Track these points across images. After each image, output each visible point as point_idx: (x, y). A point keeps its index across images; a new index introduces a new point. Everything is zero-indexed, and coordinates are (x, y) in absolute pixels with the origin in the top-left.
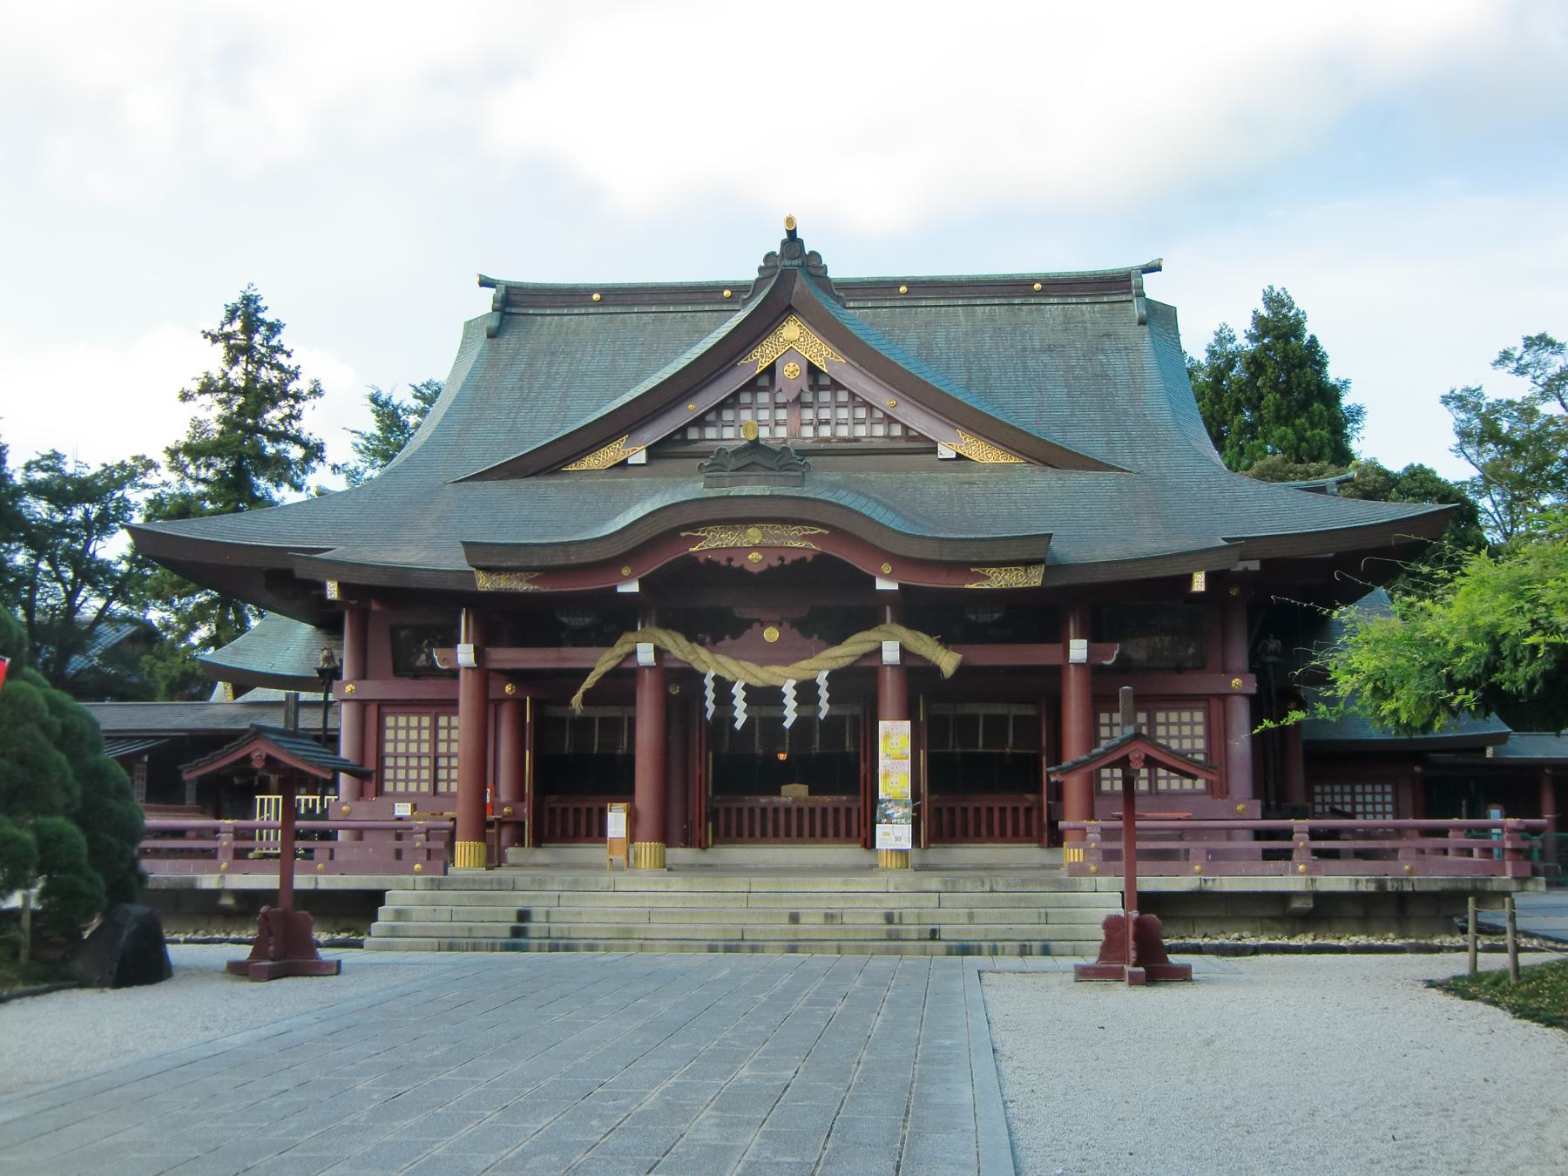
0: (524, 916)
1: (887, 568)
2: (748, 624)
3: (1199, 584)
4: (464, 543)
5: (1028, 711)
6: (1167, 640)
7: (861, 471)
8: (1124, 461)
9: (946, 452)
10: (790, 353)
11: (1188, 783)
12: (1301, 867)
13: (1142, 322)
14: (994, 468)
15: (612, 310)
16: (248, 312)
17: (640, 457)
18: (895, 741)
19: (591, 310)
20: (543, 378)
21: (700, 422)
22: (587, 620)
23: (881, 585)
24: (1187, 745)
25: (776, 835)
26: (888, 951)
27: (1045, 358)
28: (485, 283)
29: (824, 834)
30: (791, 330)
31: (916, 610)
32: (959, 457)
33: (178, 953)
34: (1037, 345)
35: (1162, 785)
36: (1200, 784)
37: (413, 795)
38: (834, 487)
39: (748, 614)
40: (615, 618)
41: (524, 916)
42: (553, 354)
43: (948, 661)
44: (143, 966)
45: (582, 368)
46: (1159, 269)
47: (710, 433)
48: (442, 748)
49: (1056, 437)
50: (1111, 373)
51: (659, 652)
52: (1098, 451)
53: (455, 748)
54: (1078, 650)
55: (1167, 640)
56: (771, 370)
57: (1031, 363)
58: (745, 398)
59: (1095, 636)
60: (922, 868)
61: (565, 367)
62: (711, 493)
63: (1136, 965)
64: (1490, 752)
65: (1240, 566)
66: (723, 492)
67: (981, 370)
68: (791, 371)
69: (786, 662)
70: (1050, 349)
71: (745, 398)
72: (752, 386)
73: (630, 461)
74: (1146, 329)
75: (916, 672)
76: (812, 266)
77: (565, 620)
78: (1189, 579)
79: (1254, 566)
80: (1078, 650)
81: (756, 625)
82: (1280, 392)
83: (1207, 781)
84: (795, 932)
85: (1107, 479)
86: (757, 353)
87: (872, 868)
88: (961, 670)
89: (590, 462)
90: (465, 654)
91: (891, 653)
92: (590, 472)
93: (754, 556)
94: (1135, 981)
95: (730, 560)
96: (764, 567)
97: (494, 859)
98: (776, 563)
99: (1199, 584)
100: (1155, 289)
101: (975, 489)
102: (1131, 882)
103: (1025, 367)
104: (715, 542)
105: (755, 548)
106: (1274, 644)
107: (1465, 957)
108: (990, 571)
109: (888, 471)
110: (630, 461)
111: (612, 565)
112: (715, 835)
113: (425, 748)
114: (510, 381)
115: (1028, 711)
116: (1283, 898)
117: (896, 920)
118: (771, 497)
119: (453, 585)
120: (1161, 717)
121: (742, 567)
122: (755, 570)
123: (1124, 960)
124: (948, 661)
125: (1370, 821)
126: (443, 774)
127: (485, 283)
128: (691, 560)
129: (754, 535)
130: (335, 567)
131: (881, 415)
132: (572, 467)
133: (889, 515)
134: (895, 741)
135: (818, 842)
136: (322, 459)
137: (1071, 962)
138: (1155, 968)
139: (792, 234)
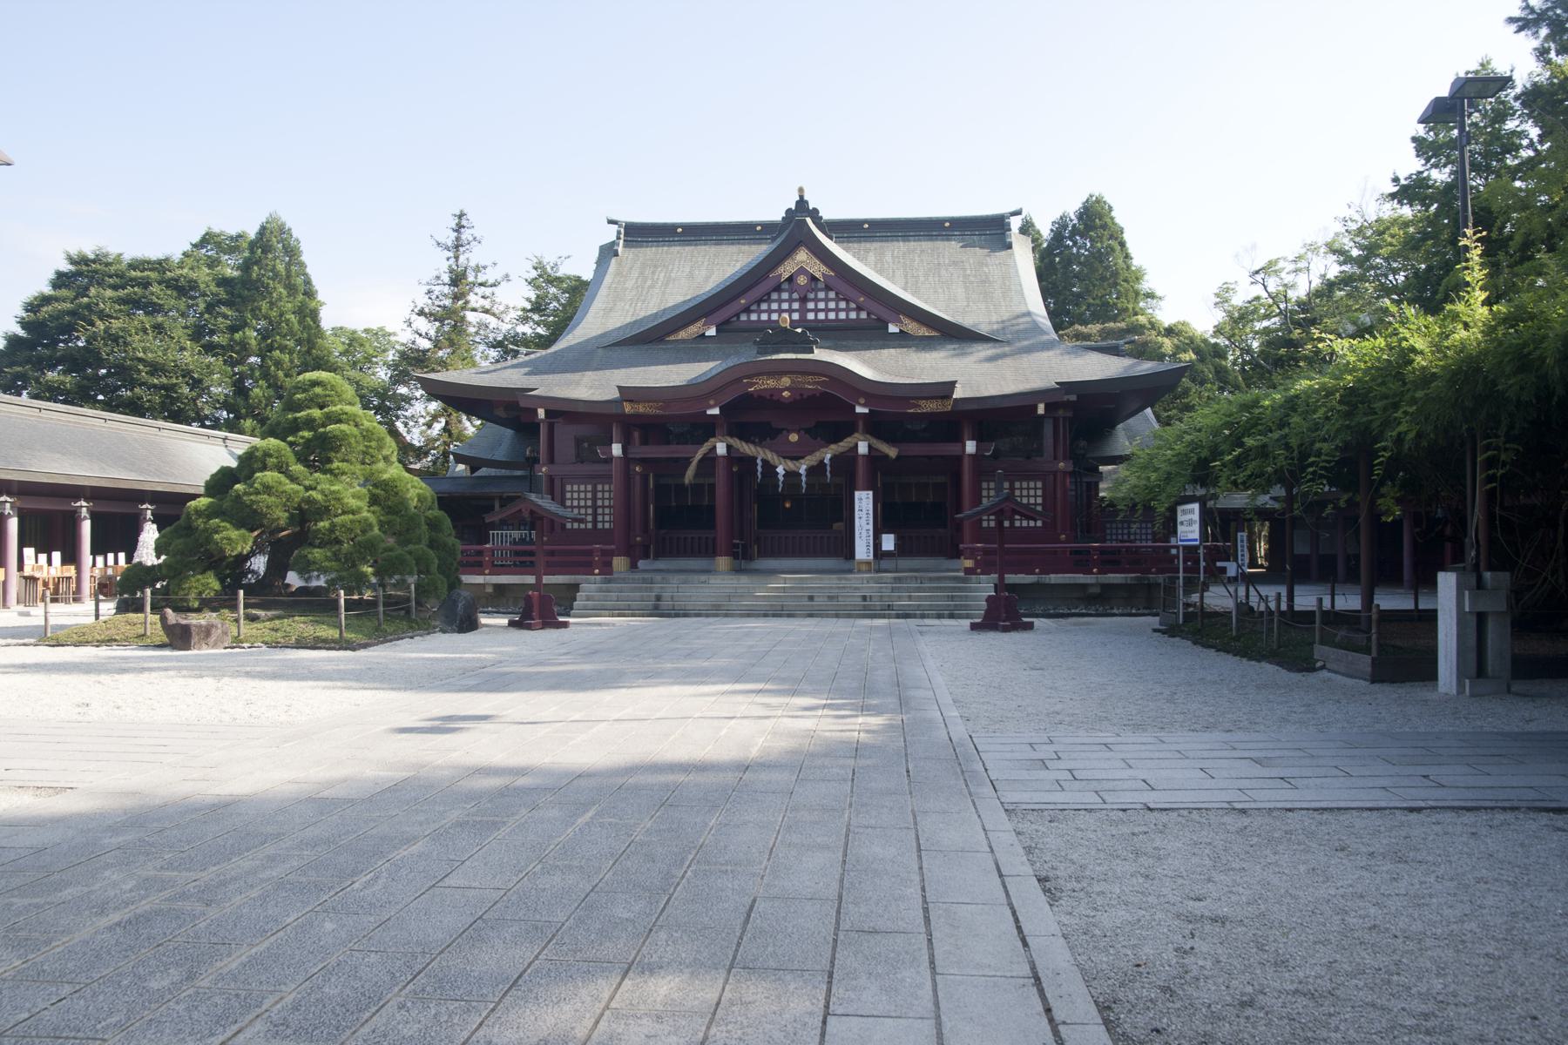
0: (658, 598)
1: (862, 401)
2: (779, 431)
3: (1041, 409)
5: (940, 479)
10: (802, 271)
11: (1032, 524)
17: (712, 332)
18: (864, 502)
21: (747, 310)
23: (859, 410)
24: (1032, 501)
28: (611, 222)
30: (802, 256)
31: (876, 426)
33: (484, 620)
35: (1017, 524)
36: (1039, 523)
40: (707, 429)
41: (658, 598)
43: (892, 452)
44: (467, 624)
47: (754, 317)
48: (599, 503)
51: (729, 447)
54: (971, 447)
56: (790, 279)
58: (775, 296)
59: (979, 439)
60: (878, 571)
65: (1066, 398)
71: (775, 296)
75: (874, 457)
78: (1035, 408)
79: (1073, 398)
80: (971, 447)
82: (1084, 267)
86: (781, 270)
87: (850, 571)
88: (898, 457)
89: (682, 335)
90: (617, 449)
92: (683, 341)
97: (633, 566)
99: (1041, 409)
102: (1001, 578)
105: (786, 389)
106: (1083, 443)
107: (815, 721)
108: (923, 403)
113: (589, 503)
114: (629, 284)
115: (940, 479)
116: (1084, 586)
124: (892, 452)
125: (1026, 343)
126: (600, 518)
127: (611, 222)
128: (750, 395)
129: (786, 381)
132: (672, 338)
134: (864, 502)
137: (966, 623)
139: (801, 197)
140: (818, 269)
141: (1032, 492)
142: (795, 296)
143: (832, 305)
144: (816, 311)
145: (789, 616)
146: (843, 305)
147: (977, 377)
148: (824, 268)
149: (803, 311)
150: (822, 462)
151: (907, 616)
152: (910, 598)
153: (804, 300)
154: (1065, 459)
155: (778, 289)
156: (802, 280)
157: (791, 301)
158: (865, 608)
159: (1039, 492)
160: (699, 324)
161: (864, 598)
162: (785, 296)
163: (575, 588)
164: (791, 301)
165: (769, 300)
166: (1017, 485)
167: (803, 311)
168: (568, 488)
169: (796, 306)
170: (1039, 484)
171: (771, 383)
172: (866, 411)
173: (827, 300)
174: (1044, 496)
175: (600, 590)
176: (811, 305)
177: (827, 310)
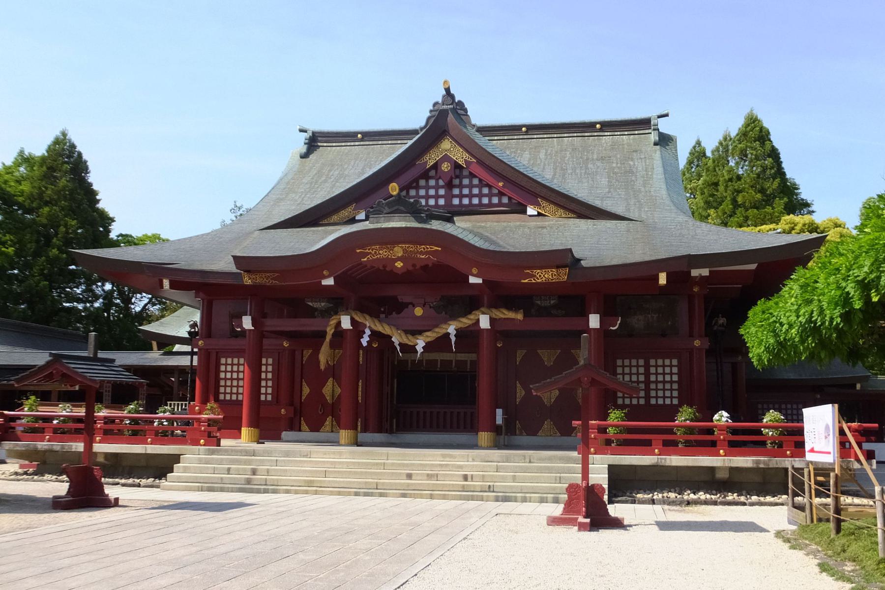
1: (475, 271)
2: (406, 305)
3: (663, 279)
4: (235, 257)
6: (655, 316)
7: (482, 222)
10: (446, 158)
12: (721, 451)
13: (656, 144)
15: (367, 143)
19: (357, 143)
20: (323, 178)
22: (323, 304)
23: (473, 280)
25: (458, 427)
26: (461, 498)
27: (599, 164)
29: (458, 427)
30: (446, 145)
34: (595, 156)
37: (627, 406)
39: (406, 299)
42: (333, 166)
45: (346, 172)
46: (667, 115)
49: (597, 203)
50: (634, 170)
52: (620, 210)
53: (241, 375)
55: (655, 316)
56: (436, 166)
57: (590, 166)
58: (422, 182)
61: (337, 172)
63: (585, 517)
64: (858, 386)
67: (562, 169)
70: (602, 159)
71: (422, 182)
73: (357, 218)
74: (658, 147)
76: (459, 110)
77: (310, 304)
81: (410, 306)
84: (408, 485)
91: (484, 322)
94: (582, 527)
95: (384, 266)
96: (405, 270)
98: (411, 268)
99: (663, 279)
100: (664, 126)
101: (545, 230)
103: (587, 168)
104: (377, 254)
105: (399, 259)
110: (357, 218)
112: (397, 426)
116: (712, 470)
117: (469, 479)
119: (230, 281)
120: (652, 362)
121: (392, 271)
123: (579, 513)
127: (301, 131)
129: (398, 251)
131: (497, 191)
133: (476, 239)
135: (447, 431)
138: (601, 521)
139: (448, 90)
140: (460, 156)
141: (667, 370)
142: (441, 183)
143: (476, 191)
144: (461, 196)
145: (381, 495)
146: (486, 191)
147: (598, 245)
148: (466, 156)
149: (449, 197)
150: (448, 335)
151: (506, 499)
152: (514, 479)
153: (449, 186)
154: (700, 337)
155: (425, 175)
156: (445, 167)
157: (437, 187)
158: (464, 489)
159: (675, 370)
160: (349, 209)
161: (465, 478)
162: (432, 182)
163: (176, 458)
164: (437, 187)
165: (417, 188)
166: (652, 362)
167: (449, 197)
168: (223, 361)
169: (442, 192)
170: (675, 362)
171: (383, 253)
172: (480, 281)
173: (471, 186)
174: (679, 374)
175: (200, 461)
176: (456, 191)
177: (471, 196)
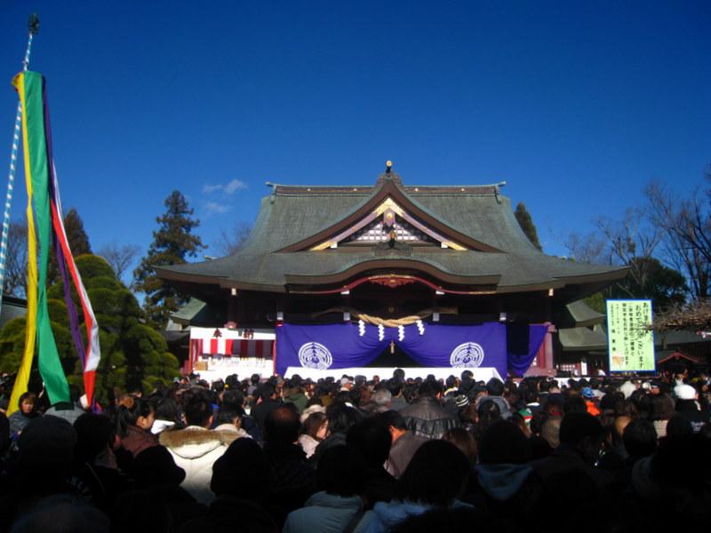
4: (285, 275)
8: (505, 248)
9: (444, 245)
14: (461, 251)
16: (176, 195)
17: (334, 246)
23: (438, 293)
30: (389, 202)
32: (449, 247)
38: (422, 257)
52: (495, 245)
56: (382, 216)
62: (378, 258)
66: (383, 257)
68: (390, 215)
69: (397, 318)
70: (470, 211)
72: (375, 222)
78: (548, 292)
83: (245, 413)
85: (504, 255)
93: (393, 281)
98: (400, 284)
99: (551, 293)
109: (425, 252)
111: (340, 285)
118: (401, 260)
122: (392, 286)
130: (235, 283)
136: (143, 259)
